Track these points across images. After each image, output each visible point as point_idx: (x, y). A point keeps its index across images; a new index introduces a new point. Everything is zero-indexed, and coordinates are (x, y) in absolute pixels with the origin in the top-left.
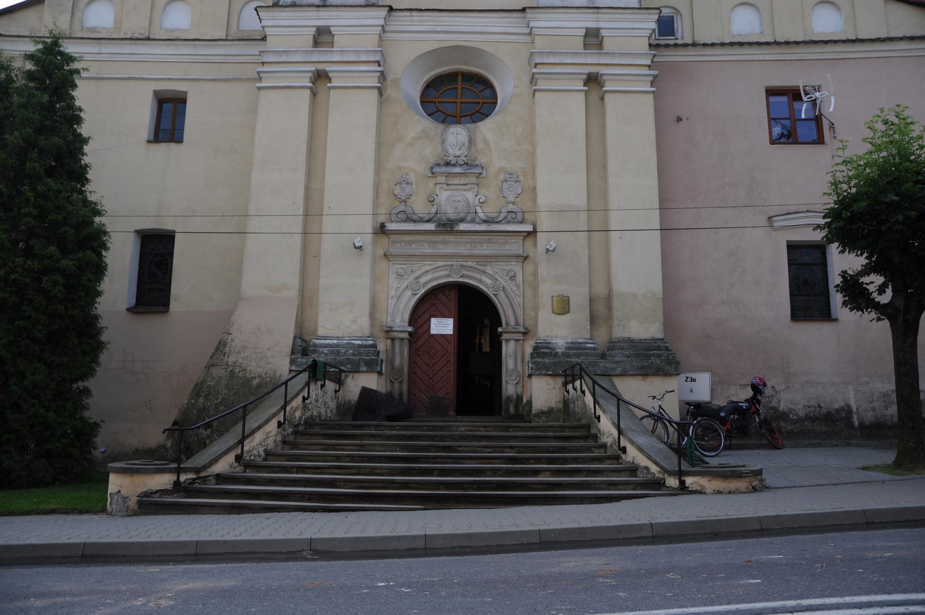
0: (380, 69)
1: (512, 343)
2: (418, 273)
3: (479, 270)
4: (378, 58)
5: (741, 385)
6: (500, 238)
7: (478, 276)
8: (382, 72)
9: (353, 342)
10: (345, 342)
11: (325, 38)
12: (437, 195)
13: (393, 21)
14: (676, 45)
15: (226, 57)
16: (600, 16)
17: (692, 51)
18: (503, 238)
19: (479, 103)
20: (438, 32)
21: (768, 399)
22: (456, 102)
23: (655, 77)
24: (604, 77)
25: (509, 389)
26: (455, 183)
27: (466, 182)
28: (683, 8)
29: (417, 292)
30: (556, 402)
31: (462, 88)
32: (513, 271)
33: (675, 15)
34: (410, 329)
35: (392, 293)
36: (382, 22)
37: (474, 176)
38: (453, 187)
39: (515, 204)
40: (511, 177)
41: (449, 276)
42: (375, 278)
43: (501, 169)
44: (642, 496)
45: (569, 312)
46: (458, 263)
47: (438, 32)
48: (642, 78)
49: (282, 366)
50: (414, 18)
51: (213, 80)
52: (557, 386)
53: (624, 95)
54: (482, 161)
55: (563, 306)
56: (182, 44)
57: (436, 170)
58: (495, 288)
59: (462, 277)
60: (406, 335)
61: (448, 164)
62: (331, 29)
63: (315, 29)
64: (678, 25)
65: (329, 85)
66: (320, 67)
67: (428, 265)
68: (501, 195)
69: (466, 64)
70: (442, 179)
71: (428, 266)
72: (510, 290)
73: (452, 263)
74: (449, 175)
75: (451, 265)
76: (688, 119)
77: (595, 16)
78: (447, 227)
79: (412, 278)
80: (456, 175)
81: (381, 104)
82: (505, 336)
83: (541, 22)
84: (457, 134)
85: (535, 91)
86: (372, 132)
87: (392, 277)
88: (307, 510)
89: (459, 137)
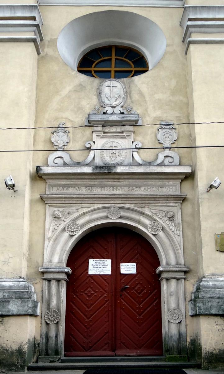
1: (173, 283)
2: (76, 215)
18: (161, 181)
29: (75, 233)
31: (116, 59)
34: (68, 270)
35: (49, 234)
41: (107, 217)
43: (156, 118)
46: (116, 205)
59: (120, 218)
73: (110, 205)
79: (69, 220)
82: (165, 276)
85: (190, 42)
87: (48, 219)
89: (115, 90)
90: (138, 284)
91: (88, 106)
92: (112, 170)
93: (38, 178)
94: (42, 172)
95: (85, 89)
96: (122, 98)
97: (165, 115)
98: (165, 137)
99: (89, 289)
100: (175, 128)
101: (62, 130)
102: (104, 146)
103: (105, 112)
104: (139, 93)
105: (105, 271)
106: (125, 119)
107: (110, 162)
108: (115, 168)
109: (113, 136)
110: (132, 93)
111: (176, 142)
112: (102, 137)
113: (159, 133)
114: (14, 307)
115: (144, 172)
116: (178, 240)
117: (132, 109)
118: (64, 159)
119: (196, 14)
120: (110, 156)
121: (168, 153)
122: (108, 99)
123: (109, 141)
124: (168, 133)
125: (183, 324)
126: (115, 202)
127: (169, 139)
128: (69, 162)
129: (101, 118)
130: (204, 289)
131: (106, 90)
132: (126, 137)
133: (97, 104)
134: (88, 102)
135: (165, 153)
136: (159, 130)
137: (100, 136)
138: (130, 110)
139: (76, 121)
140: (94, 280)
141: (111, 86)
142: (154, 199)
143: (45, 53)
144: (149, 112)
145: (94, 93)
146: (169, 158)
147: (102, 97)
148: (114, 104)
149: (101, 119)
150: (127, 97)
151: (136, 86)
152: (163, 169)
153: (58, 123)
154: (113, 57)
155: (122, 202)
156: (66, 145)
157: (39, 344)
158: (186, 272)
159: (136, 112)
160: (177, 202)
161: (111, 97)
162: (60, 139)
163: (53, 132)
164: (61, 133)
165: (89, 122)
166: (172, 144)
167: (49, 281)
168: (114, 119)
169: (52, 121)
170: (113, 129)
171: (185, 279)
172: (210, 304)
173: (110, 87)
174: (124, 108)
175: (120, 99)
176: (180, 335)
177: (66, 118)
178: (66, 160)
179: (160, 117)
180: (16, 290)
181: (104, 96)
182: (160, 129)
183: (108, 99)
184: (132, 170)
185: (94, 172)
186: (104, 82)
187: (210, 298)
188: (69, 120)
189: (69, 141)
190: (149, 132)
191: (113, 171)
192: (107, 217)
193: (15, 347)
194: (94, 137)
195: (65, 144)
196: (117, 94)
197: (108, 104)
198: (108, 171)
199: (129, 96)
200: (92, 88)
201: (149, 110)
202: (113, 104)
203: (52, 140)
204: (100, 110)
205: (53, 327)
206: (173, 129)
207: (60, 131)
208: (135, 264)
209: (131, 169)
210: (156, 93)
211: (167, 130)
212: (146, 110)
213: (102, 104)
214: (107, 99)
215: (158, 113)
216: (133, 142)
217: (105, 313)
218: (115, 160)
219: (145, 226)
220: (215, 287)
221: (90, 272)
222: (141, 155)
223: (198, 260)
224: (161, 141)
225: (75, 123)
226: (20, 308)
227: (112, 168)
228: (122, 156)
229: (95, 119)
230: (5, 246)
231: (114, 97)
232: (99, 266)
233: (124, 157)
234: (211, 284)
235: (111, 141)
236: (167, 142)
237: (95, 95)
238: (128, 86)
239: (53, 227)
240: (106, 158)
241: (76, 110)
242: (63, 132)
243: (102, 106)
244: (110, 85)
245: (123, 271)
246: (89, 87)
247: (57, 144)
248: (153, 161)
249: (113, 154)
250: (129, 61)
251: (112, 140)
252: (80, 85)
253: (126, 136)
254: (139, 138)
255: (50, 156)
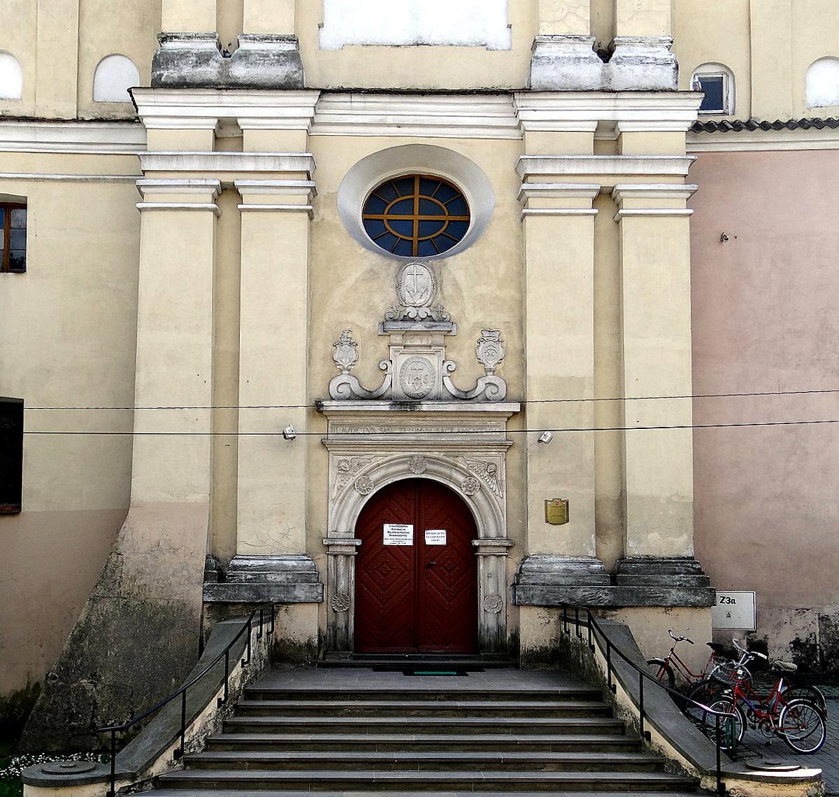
0: (311, 184)
1: (493, 560)
2: (367, 467)
3: (447, 462)
4: (306, 167)
5: (797, 610)
6: (476, 419)
7: (448, 471)
8: (313, 189)
9: (285, 562)
10: (275, 562)
11: (229, 132)
12: (391, 361)
13: (326, 108)
14: (723, 127)
15: (80, 146)
16: (619, 103)
17: (746, 136)
18: (481, 419)
19: (444, 221)
20: (389, 125)
21: (833, 629)
22: (412, 221)
23: (693, 193)
24: (622, 194)
25: (488, 619)
26: (415, 343)
27: (430, 343)
28: (738, 66)
29: (367, 493)
30: (551, 640)
31: (420, 199)
32: (493, 464)
33: (724, 76)
34: (359, 542)
35: (334, 494)
36: (310, 113)
37: (441, 335)
38: (413, 350)
39: (496, 372)
40: (488, 335)
41: (409, 471)
42: (309, 474)
43: (476, 325)
44: (295, 765)
45: (568, 521)
46: (420, 453)
47: (389, 125)
48: (674, 195)
49: (196, 596)
50: (354, 105)
51: (63, 180)
52: (552, 620)
53: (648, 219)
54: (452, 313)
55: (559, 513)
56: (14, 127)
57: (390, 326)
58: (470, 488)
59: (426, 471)
60: (352, 550)
61: (406, 319)
62: (240, 121)
63: (216, 121)
64: (728, 92)
65: (240, 206)
66: (227, 178)
67: (380, 457)
68: (477, 360)
69: (425, 165)
70: (397, 339)
71: (381, 458)
72: (488, 489)
73: (413, 453)
74: (406, 333)
75: (412, 457)
76: (736, 237)
77: (612, 103)
78: (407, 404)
79: (358, 474)
80: (416, 333)
81: (311, 229)
82: (482, 550)
83: (536, 111)
84: (417, 274)
85: (525, 215)
86: (303, 273)
87: (333, 472)
88: (79, 783)
89: (420, 279)
90: (448, 559)
91: (382, 305)
93: (317, 413)
99: (385, 565)
105: (405, 541)
114: (300, 592)
116: (501, 503)
119: (536, 167)
121: (491, 379)
125: (503, 613)
126: (419, 450)
130: (526, 573)
131: (408, 280)
134: (382, 299)
140: (389, 551)
141: (415, 273)
142: (414, 738)
143: (321, 218)
148: (419, 302)
154: (417, 196)
155: (429, 450)
157: (325, 637)
158: (508, 548)
160: (500, 450)
162: (344, 356)
167: (335, 556)
171: (506, 556)
172: (532, 592)
176: (499, 627)
179: (482, 323)
180: (301, 571)
187: (533, 584)
192: (409, 471)
193: (303, 641)
205: (341, 616)
208: (444, 531)
215: (479, 317)
217: (397, 578)
219: (459, 485)
220: (541, 571)
221: (386, 542)
223: (524, 533)
226: (308, 594)
230: (283, 513)
232: (397, 534)
234: (535, 566)
239: (339, 484)
241: (366, 311)
245: (429, 541)
250: (440, 203)
252: (372, 270)
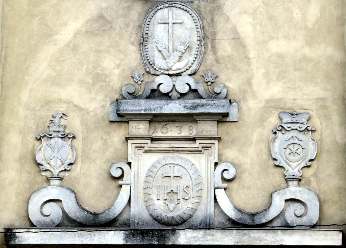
89: (179, 31)
91: (117, 72)
92: (167, 239)
94: (17, 242)
95: (111, 27)
96: (194, 52)
97: (291, 95)
98: (288, 151)
100: (313, 129)
101: (59, 132)
102: (151, 174)
103: (156, 88)
104: (233, 39)
106: (199, 110)
107: (164, 214)
108: (174, 234)
109: (172, 149)
110: (218, 37)
111: (314, 163)
112: (149, 151)
113: (276, 140)
115: (236, 244)
117: (217, 79)
118: (64, 205)
120: (165, 200)
121: (295, 192)
122: (162, 54)
123: (164, 163)
124: (296, 141)
127: (297, 157)
128: (75, 212)
129: (145, 108)
132: (201, 151)
133: (137, 66)
134: (118, 62)
135: (288, 192)
136: (275, 133)
137: (143, 147)
138: (212, 83)
139: (91, 109)
141: (171, 21)
144: (255, 88)
145: (131, 38)
146: (297, 205)
147: (149, 49)
148: (177, 67)
149: (145, 110)
150: (206, 48)
151: (228, 19)
152: (278, 238)
153: (50, 114)
156: (68, 171)
159: (225, 87)
161: (168, 51)
163: (38, 137)
164: (56, 139)
165: (119, 115)
166: (306, 169)
168: (175, 111)
169: (38, 108)
170: (173, 131)
173: (167, 25)
174: (197, 76)
175: (190, 55)
177: (68, 102)
178: (68, 207)
179: (280, 100)
181: (154, 46)
182: (279, 131)
183: (162, 54)
184: (211, 240)
185: (129, 244)
186: (153, 12)
188: (75, 105)
189: (74, 162)
190: (255, 137)
191: (169, 240)
194: (129, 152)
195: (65, 167)
196: (183, 44)
197: (162, 68)
198: (158, 241)
199: (210, 45)
200: (127, 25)
201: (254, 81)
202: (173, 68)
203: (36, 157)
204: (144, 83)
206: (309, 131)
207: (55, 134)
209: (209, 238)
210: (273, 38)
211: (294, 133)
212: (249, 83)
213: (150, 66)
214: (160, 56)
216: (216, 164)
218: (176, 210)
222: (234, 194)
224: (281, 162)
225: (88, 113)
227: (167, 235)
228: (191, 200)
229: (132, 110)
231: (177, 50)
233: (196, 201)
235: (167, 162)
236: (294, 164)
237: (133, 44)
238: (209, 20)
240: (156, 202)
241: (91, 82)
242: (62, 138)
243: (148, 73)
244: (168, 18)
246: (119, 23)
247: (48, 166)
248: (261, 209)
249: (172, 194)
251: (170, 158)
252: (101, 17)
253: (200, 149)
254: (231, 153)
255: (32, 197)
